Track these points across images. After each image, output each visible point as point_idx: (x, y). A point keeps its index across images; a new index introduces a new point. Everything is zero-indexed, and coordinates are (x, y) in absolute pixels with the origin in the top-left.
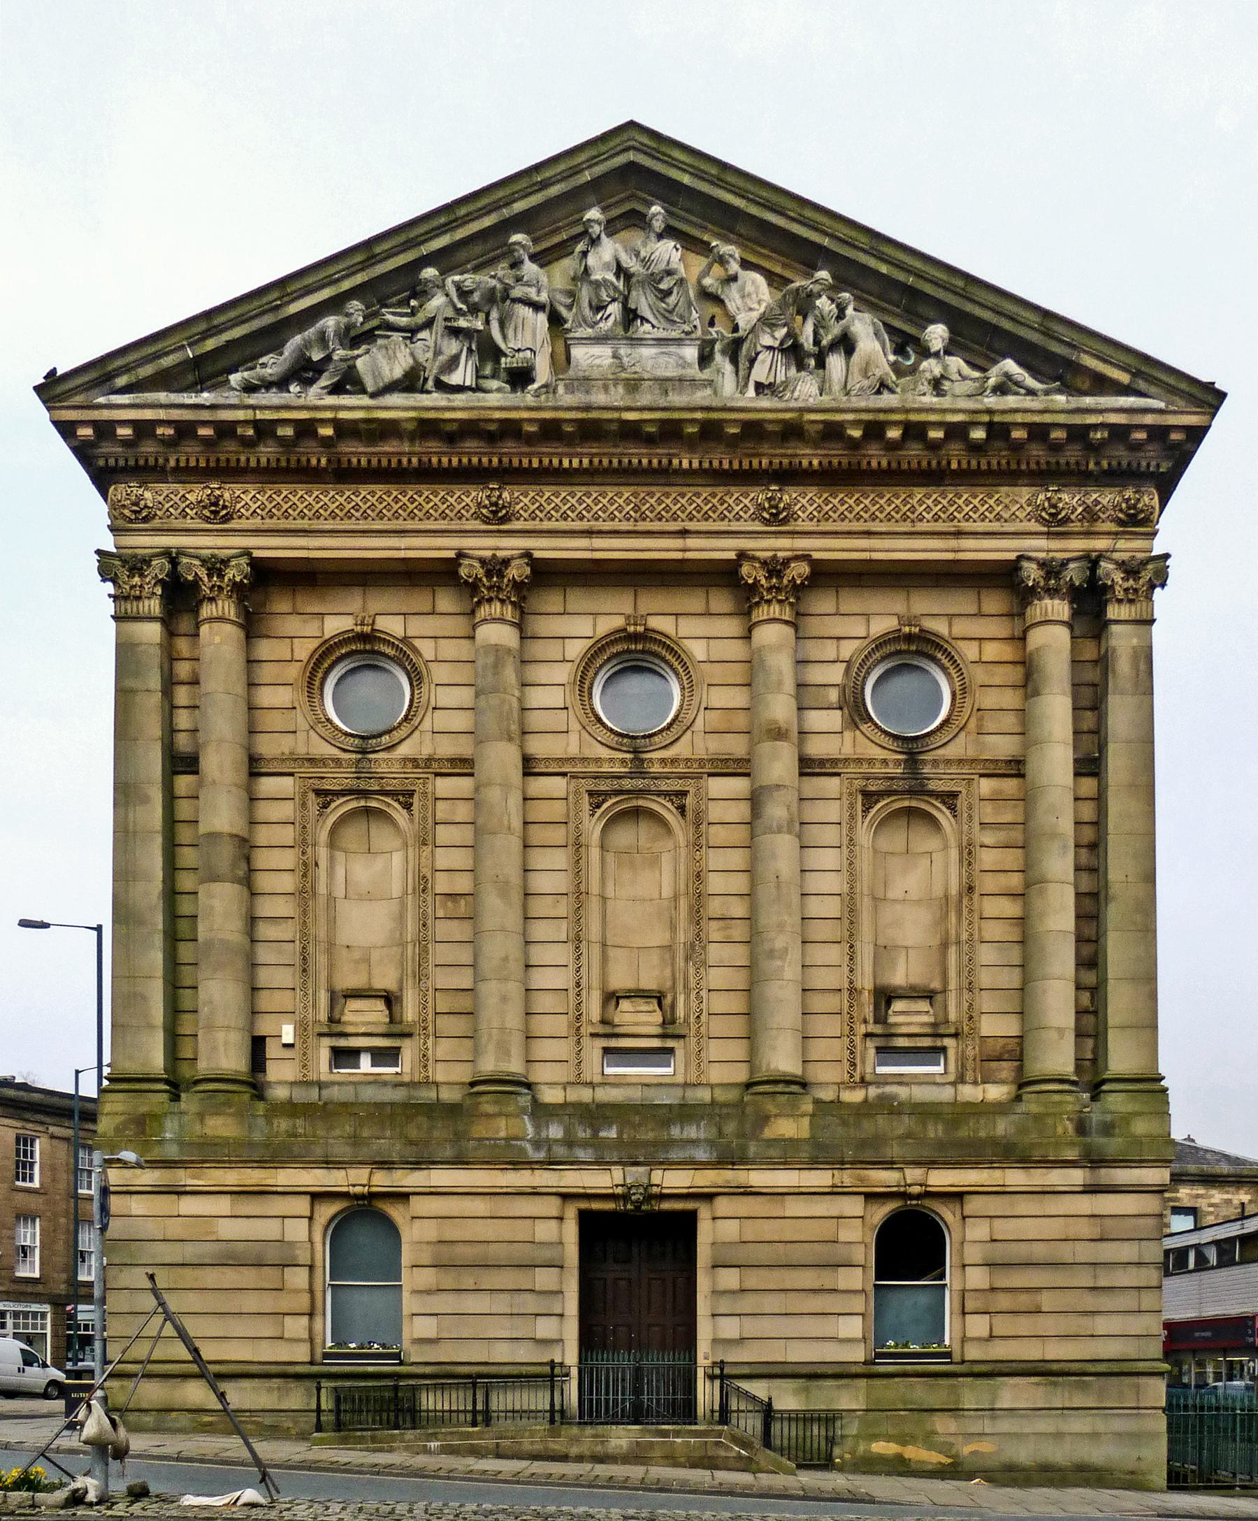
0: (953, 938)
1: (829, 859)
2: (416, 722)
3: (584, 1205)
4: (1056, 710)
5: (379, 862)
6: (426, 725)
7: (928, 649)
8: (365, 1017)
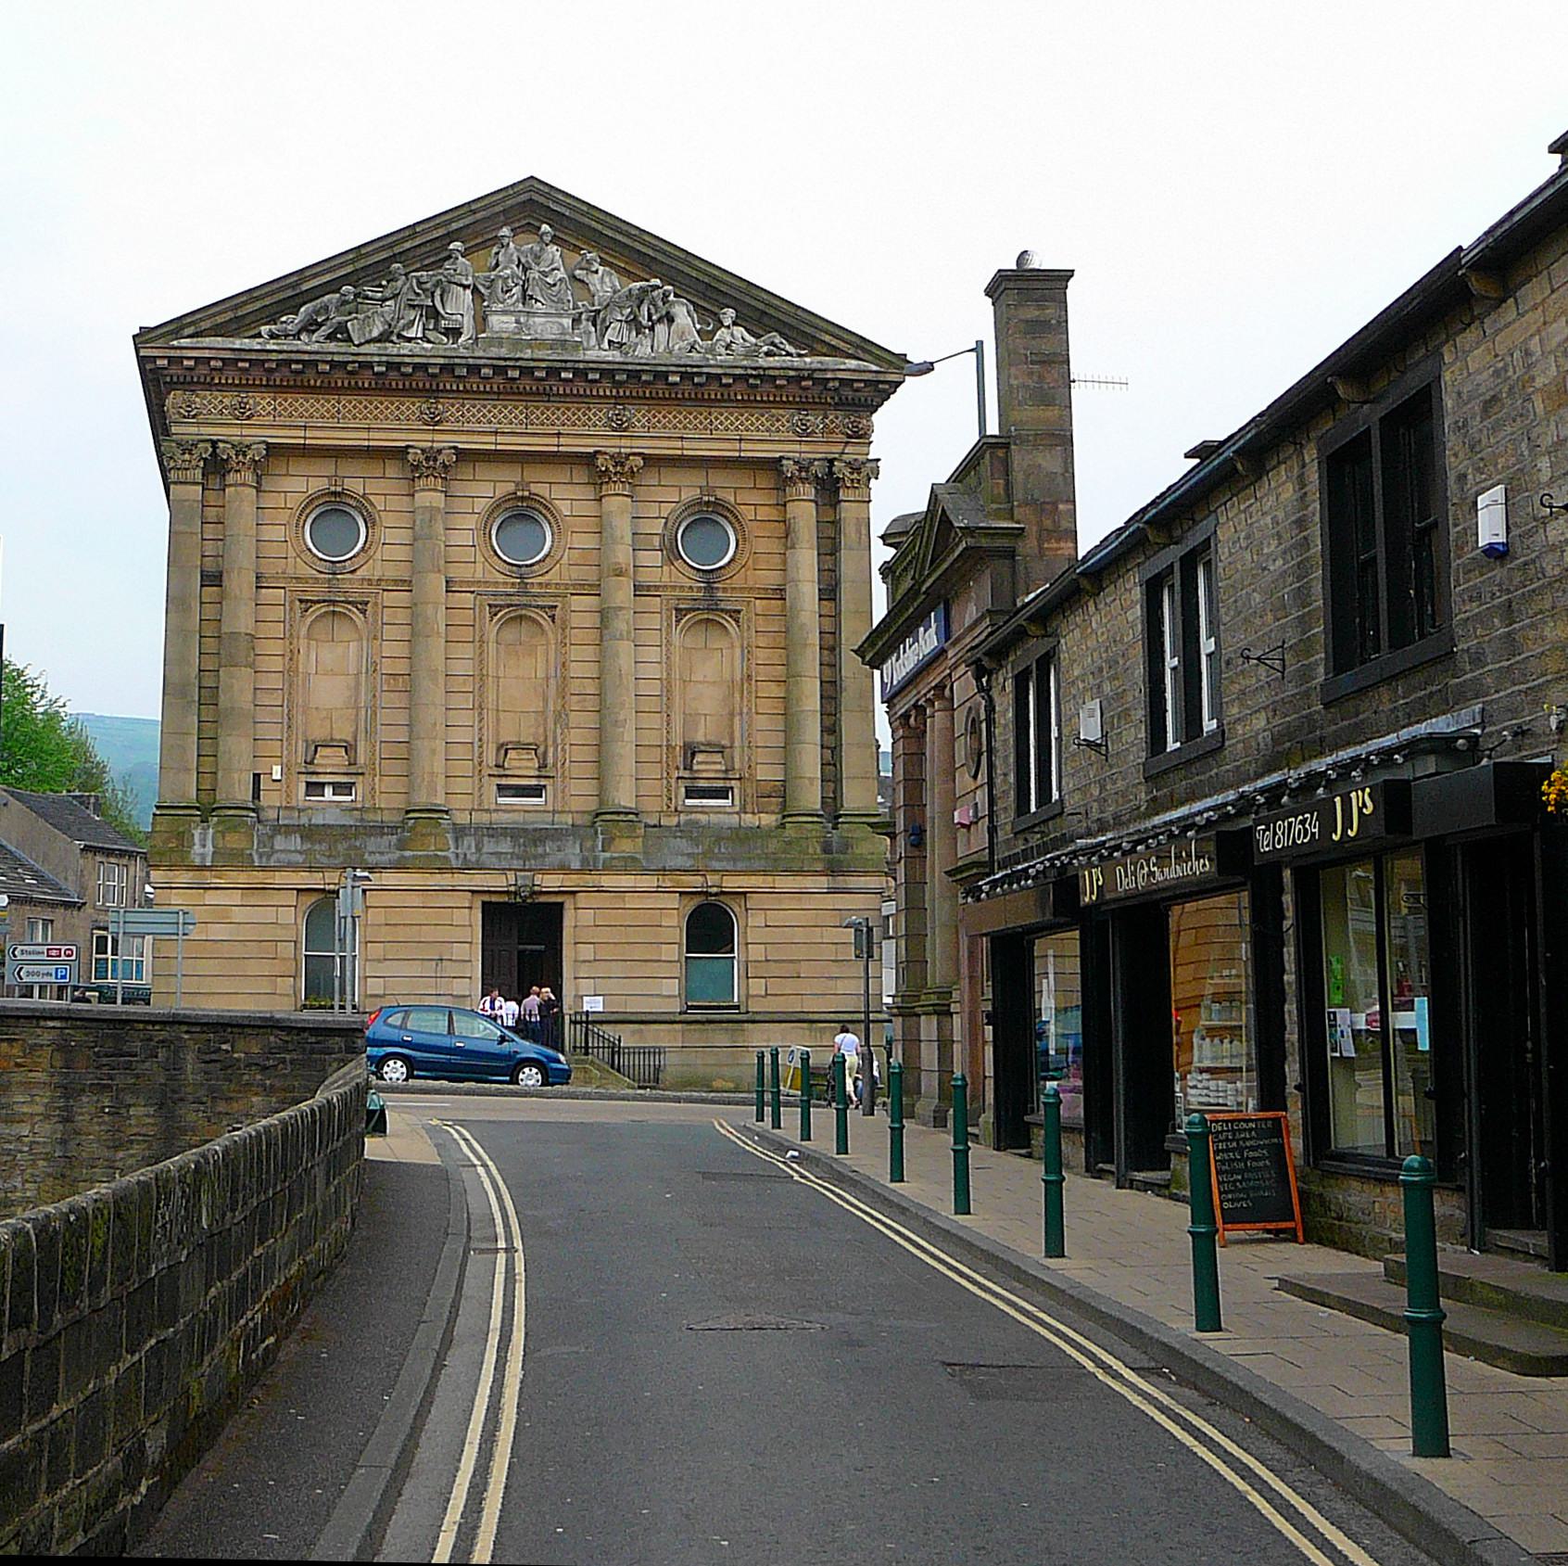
0: (737, 710)
1: (653, 654)
2: (371, 552)
3: (486, 898)
4: (806, 561)
5: (340, 649)
6: (378, 555)
7: (720, 510)
8: (331, 761)
